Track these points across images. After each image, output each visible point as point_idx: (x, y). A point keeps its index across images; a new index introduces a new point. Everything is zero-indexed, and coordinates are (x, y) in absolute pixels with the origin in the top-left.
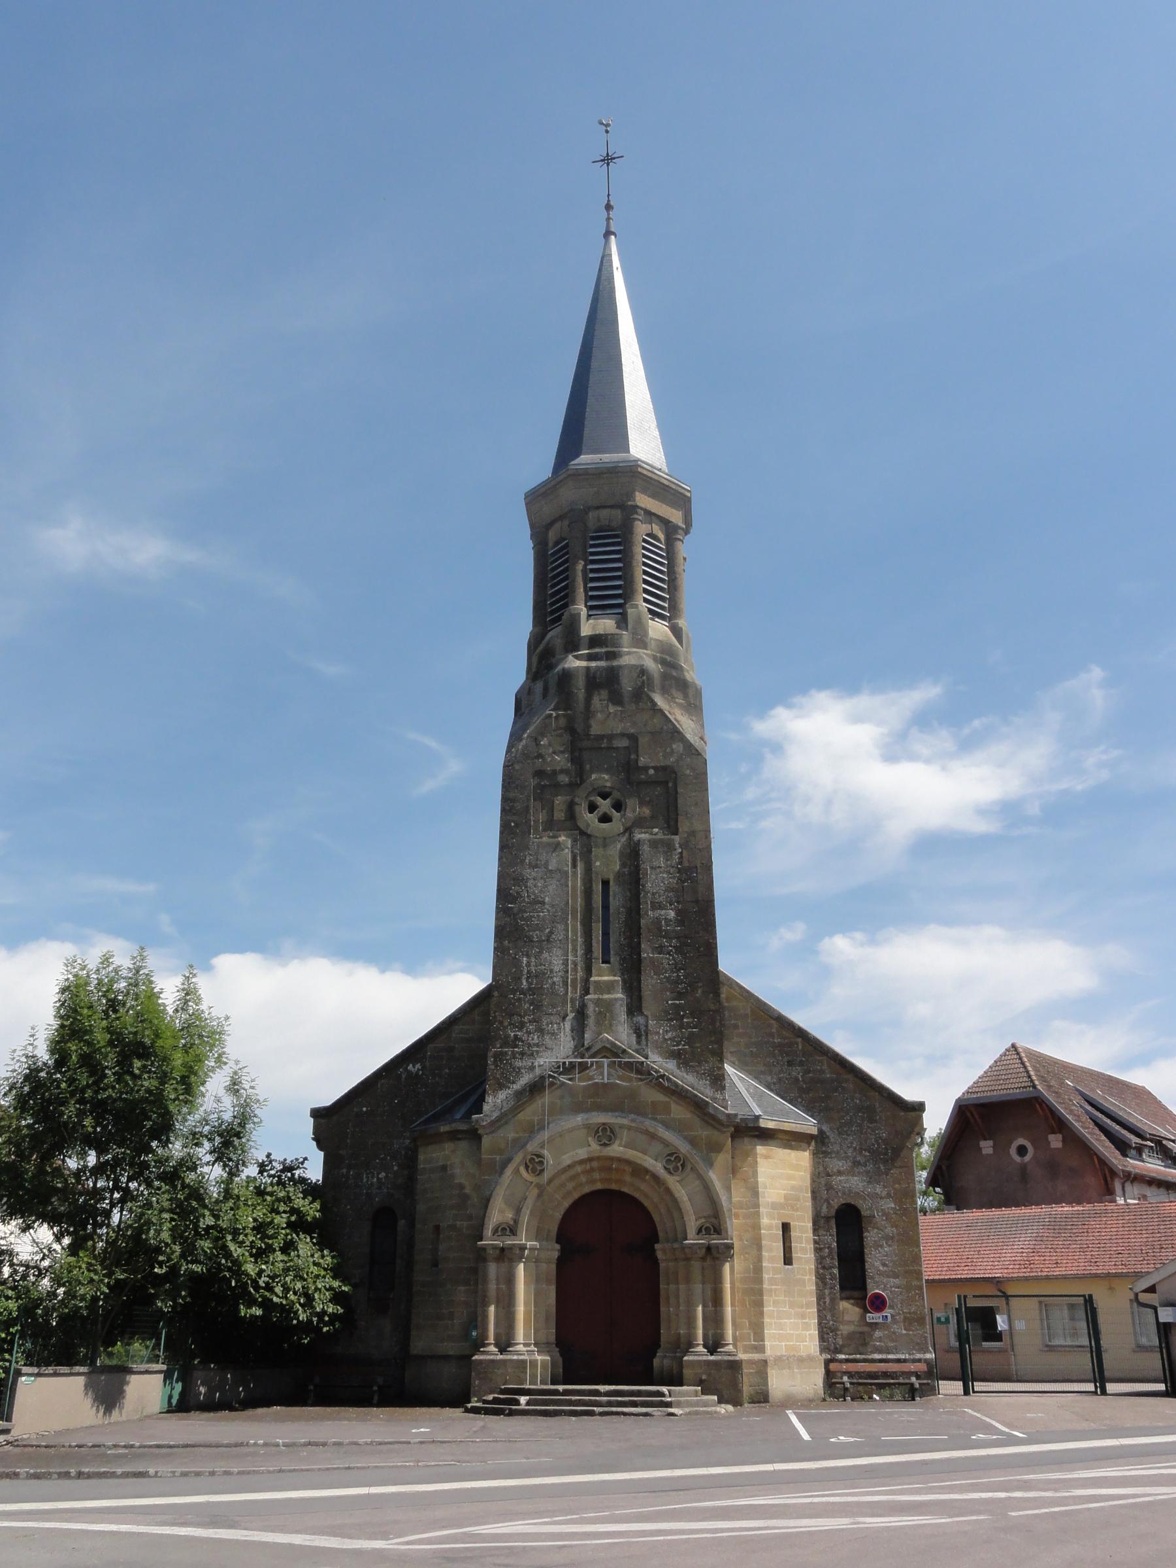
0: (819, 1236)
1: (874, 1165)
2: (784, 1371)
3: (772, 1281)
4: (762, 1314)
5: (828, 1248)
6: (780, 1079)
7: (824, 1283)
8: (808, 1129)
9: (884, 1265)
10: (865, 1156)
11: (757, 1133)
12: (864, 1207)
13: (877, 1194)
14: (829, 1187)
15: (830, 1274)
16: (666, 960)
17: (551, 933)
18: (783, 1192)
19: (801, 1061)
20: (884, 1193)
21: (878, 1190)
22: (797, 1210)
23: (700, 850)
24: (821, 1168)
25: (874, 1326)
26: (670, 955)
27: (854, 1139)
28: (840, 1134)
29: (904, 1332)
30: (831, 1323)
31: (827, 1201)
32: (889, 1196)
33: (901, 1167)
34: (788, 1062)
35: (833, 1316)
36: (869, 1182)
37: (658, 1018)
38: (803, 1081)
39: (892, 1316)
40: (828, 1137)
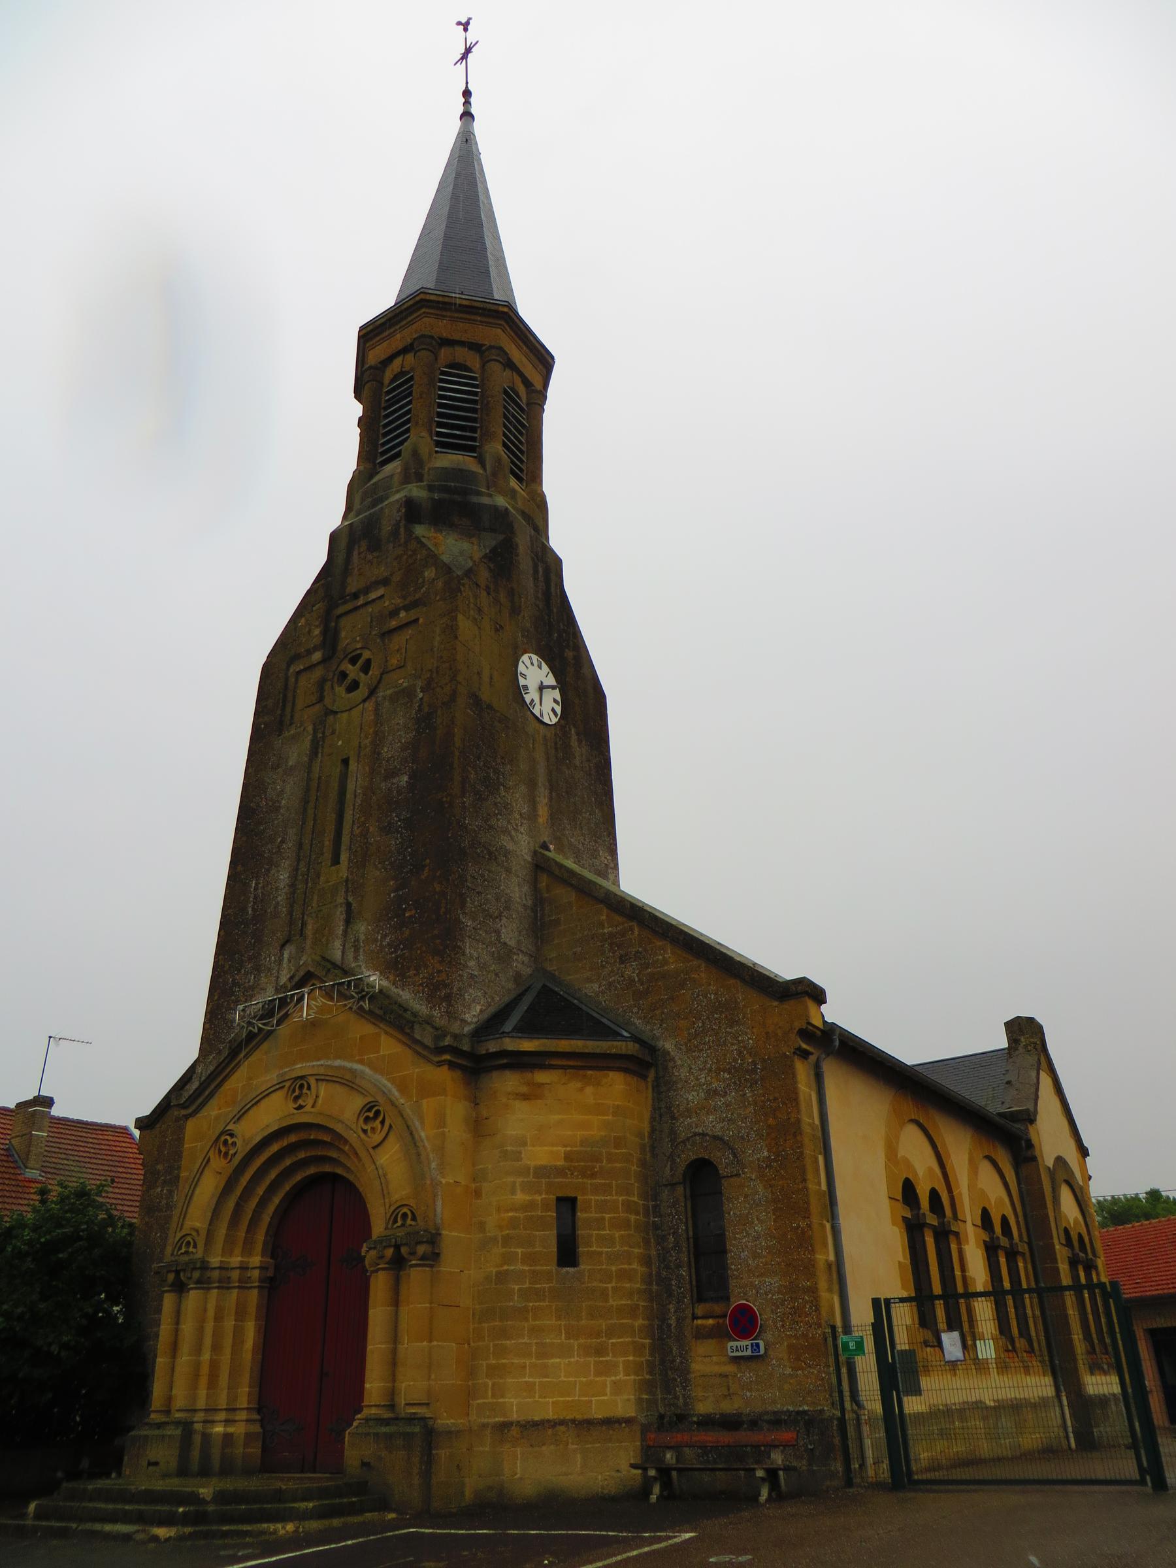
2: (544, 1448)
5: (674, 1233)
9: (755, 1256)
10: (725, 1080)
17: (282, 842)
19: (638, 952)
22: (593, 1175)
27: (708, 1056)
34: (620, 958)
38: (639, 980)
40: (673, 1060)
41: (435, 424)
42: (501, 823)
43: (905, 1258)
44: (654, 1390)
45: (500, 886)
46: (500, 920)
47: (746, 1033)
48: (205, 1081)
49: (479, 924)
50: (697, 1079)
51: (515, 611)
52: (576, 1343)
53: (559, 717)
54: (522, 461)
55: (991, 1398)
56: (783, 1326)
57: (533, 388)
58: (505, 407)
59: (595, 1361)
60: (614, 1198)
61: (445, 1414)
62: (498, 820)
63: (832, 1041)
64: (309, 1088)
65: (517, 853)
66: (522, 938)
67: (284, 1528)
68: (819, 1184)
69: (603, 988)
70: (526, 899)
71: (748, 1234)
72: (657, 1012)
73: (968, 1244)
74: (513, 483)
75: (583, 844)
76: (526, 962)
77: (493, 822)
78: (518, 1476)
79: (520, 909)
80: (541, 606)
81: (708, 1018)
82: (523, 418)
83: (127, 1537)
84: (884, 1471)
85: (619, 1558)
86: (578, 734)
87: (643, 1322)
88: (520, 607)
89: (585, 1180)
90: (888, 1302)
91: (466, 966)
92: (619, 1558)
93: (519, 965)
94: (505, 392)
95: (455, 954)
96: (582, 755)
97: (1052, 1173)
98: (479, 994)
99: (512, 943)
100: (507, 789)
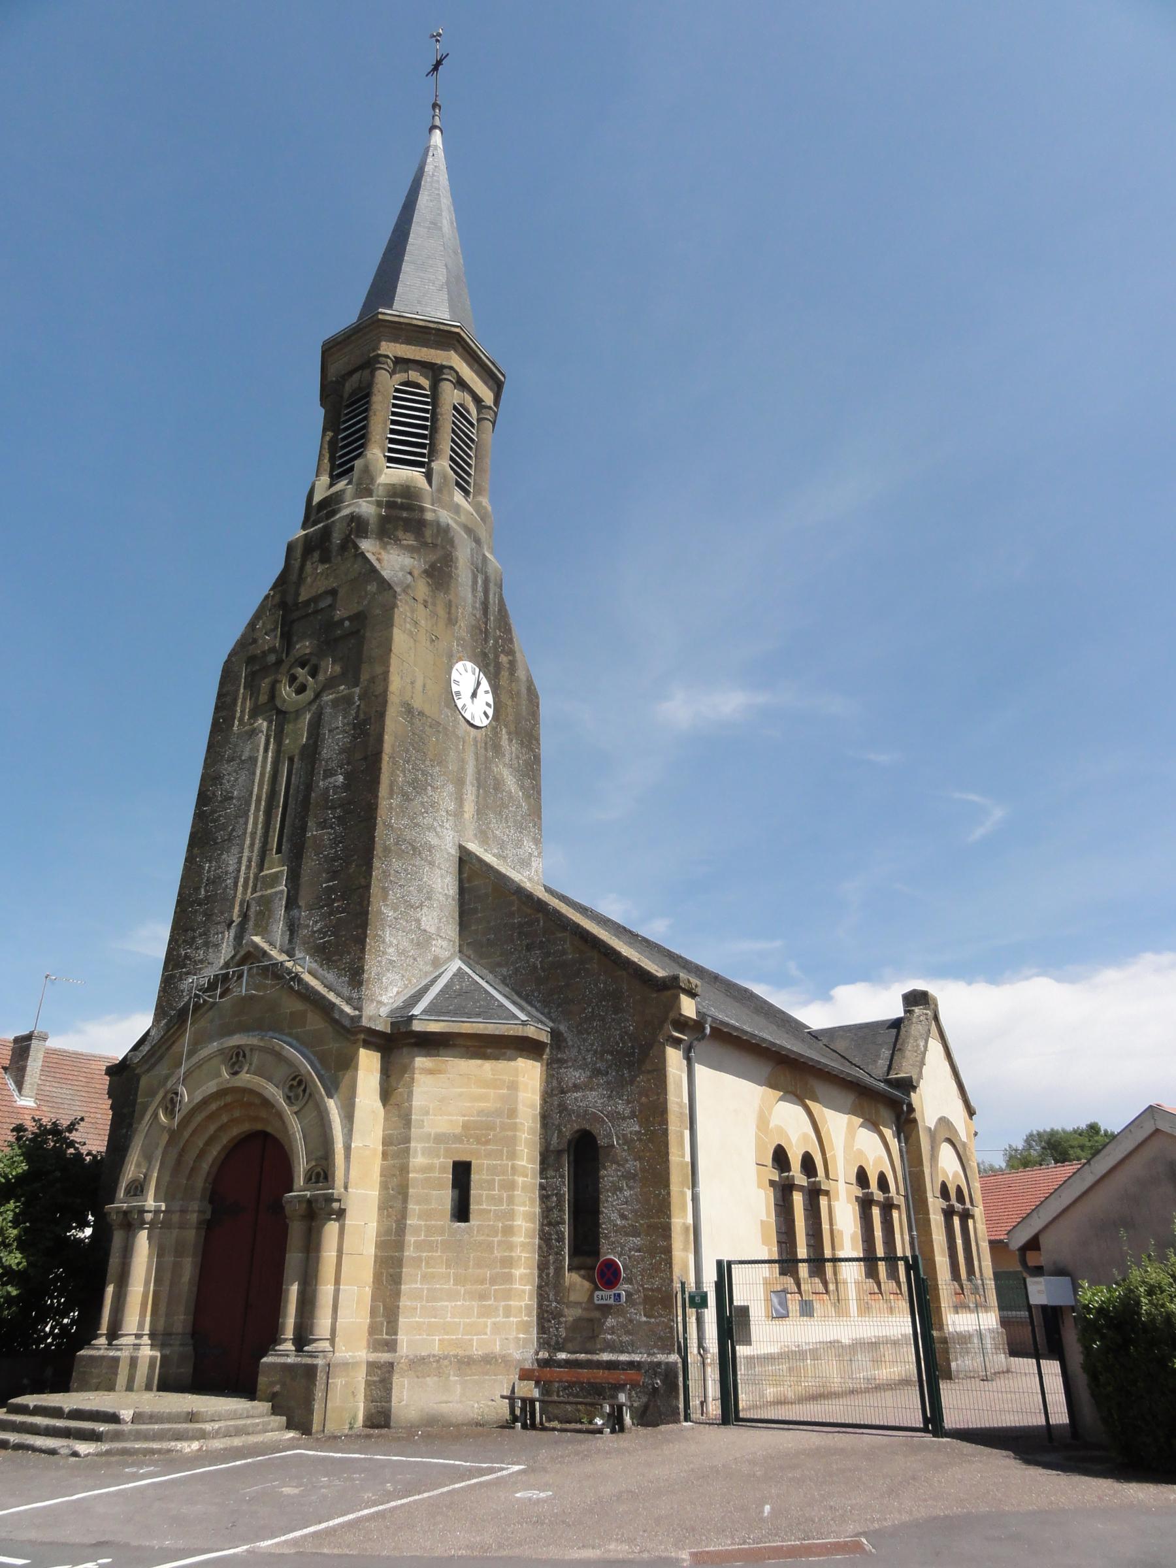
0: (546, 1178)
1: (617, 1072)
2: (428, 1379)
3: (419, 1246)
4: (397, 1294)
5: (556, 1195)
6: (517, 970)
7: (549, 1246)
8: (508, 1030)
9: (623, 1217)
10: (607, 1061)
11: (413, 1041)
12: (599, 1131)
13: (618, 1113)
14: (563, 1108)
15: (557, 1233)
16: (326, 835)
17: (233, 830)
18: (462, 1118)
19: (541, 942)
20: (627, 1112)
21: (620, 1108)
22: (487, 1142)
23: (376, 696)
24: (555, 1083)
25: (605, 1310)
26: (332, 828)
28: (580, 1033)
29: (644, 1319)
30: (554, 1304)
31: (558, 1127)
32: (633, 1115)
33: (649, 1072)
35: (556, 1295)
36: (610, 1097)
37: (310, 908)
38: (541, 968)
39: (629, 1295)
40: (565, 1040)
41: (388, 441)
42: (428, 820)
43: (768, 1215)
44: (531, 1329)
45: (422, 879)
46: (421, 909)
47: (628, 1020)
48: (155, 1045)
49: (401, 914)
50: (585, 1059)
51: (451, 621)
52: (463, 1288)
53: (490, 719)
54: (469, 474)
55: (850, 1337)
56: (642, 1280)
57: (483, 403)
58: (454, 423)
59: (478, 1304)
60: (505, 1162)
61: (344, 1348)
62: (424, 818)
63: (704, 1029)
64: (244, 1056)
65: (442, 847)
66: (442, 924)
67: (189, 1446)
68: (683, 1156)
69: (511, 972)
70: (448, 890)
71: (618, 1199)
72: (556, 997)
73: (838, 1200)
74: (458, 497)
75: (508, 835)
76: (444, 946)
77: (420, 819)
78: (404, 1402)
79: (442, 898)
80: (478, 616)
81: (597, 1005)
82: (472, 433)
83: (52, 1452)
84: (714, 1408)
85: (445, 1489)
86: (509, 733)
87: (525, 1271)
88: (457, 617)
89: (479, 1146)
90: (730, 1263)
91: (384, 953)
92: (445, 1489)
93: (437, 949)
94: (455, 408)
95: (375, 943)
96: (512, 753)
97: (932, 1134)
98: (397, 977)
99: (432, 930)
100: (434, 789)
